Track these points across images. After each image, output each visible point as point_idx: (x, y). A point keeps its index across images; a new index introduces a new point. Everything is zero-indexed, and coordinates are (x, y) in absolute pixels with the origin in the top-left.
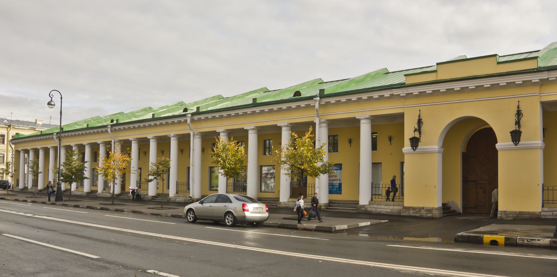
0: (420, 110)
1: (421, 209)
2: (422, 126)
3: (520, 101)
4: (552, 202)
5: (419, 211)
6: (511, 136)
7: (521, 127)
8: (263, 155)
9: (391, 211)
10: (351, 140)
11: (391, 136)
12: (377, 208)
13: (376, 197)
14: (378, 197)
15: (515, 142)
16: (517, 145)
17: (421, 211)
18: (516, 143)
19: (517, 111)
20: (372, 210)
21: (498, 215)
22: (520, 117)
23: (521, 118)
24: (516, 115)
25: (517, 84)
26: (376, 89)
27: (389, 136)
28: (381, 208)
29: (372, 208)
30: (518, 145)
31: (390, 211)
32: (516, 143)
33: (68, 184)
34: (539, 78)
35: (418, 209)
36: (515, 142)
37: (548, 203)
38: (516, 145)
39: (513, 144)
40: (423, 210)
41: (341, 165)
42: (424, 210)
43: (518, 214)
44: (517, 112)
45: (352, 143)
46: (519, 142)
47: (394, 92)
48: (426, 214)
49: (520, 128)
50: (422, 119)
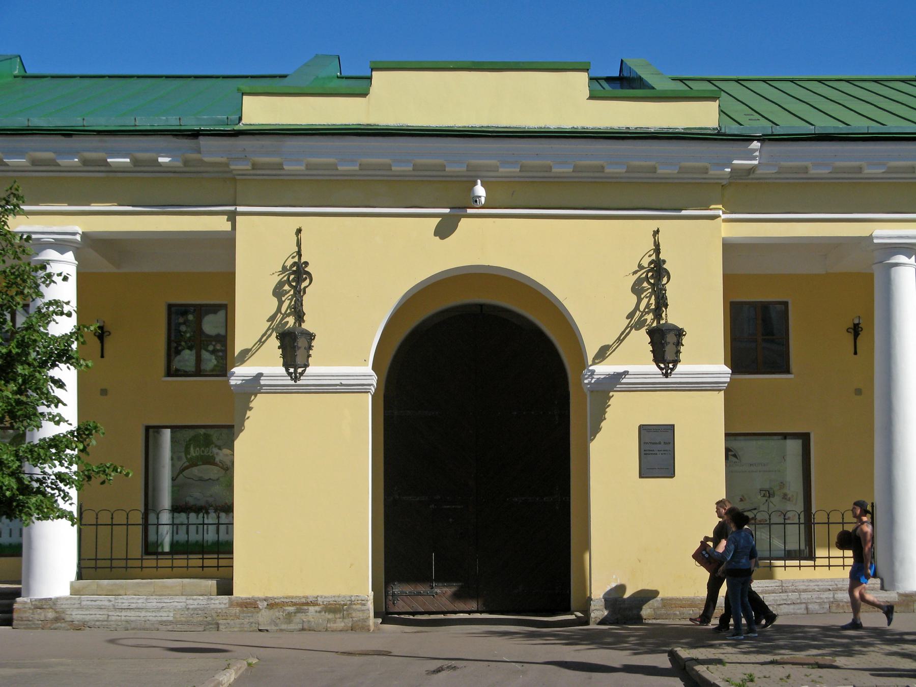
1: (307, 604)
4: (123, 563)
5: (299, 611)
6: (652, 343)
8: (165, 377)
9: (174, 617)
13: (207, 563)
14: (214, 563)
15: (662, 366)
17: (305, 612)
18: (667, 368)
20: (88, 618)
21: (593, 615)
26: (643, 136)
28: (133, 606)
29: (88, 608)
30: (672, 376)
31: (171, 619)
32: (667, 368)
35: (294, 604)
36: (662, 366)
37: (96, 568)
38: (666, 375)
39: (658, 370)
40: (312, 609)
41: (148, 428)
42: (317, 608)
43: (658, 608)
46: (675, 366)
48: (329, 621)
49: (304, 321)
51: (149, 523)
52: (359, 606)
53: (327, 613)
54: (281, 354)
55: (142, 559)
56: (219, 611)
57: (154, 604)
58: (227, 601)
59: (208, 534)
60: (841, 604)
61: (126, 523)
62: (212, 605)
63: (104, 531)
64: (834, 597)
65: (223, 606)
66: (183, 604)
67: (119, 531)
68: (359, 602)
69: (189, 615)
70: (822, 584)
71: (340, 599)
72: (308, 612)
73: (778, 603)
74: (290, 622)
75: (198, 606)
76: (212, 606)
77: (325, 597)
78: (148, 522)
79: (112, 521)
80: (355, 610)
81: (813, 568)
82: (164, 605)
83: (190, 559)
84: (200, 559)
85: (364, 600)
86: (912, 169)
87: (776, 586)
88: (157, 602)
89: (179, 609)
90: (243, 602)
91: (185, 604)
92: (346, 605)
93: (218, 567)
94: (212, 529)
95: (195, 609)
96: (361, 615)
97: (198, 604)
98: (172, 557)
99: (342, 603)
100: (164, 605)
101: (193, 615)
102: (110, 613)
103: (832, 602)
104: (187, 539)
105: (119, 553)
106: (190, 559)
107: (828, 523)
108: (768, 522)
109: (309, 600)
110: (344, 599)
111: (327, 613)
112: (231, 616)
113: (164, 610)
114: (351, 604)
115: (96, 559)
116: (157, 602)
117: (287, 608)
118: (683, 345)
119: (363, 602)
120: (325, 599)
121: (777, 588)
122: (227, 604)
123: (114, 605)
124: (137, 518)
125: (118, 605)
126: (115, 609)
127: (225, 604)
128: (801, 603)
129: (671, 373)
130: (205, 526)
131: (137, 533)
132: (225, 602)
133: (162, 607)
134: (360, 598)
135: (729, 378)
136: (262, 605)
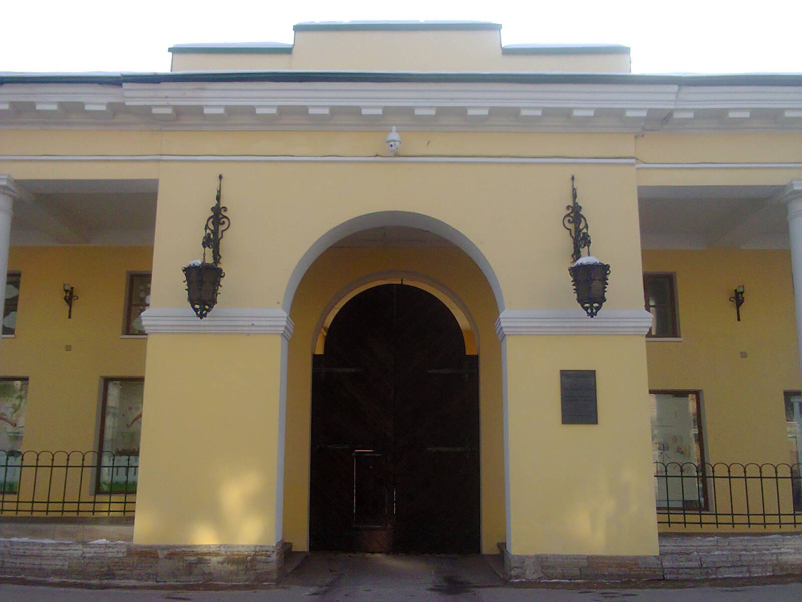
0: (221, 177)
2: (224, 233)
3: (223, 176)
7: (221, 261)
9: (69, 567)
10: (75, 293)
11: (72, 288)
12: (33, 550)
16: (205, 316)
19: (213, 209)
22: (222, 228)
23: (223, 231)
24: (208, 220)
25: (261, 115)
27: (67, 288)
28: (29, 553)
33: (574, 289)
34: (648, 106)
36: (197, 306)
44: (212, 214)
45: (75, 303)
47: (127, 94)
50: (225, 209)
51: (103, 465)
52: (264, 558)
53: (230, 565)
54: (572, 282)
55: (794, 515)
56: (116, 560)
57: (49, 552)
58: (125, 549)
59: (117, 475)
60: (785, 567)
61: (51, 465)
62: (110, 553)
63: (59, 473)
64: (777, 559)
65: (120, 555)
66: (80, 553)
67: (43, 473)
68: (264, 553)
69: (85, 564)
70: (761, 544)
71: (243, 549)
72: (210, 563)
73: (718, 565)
74: (190, 573)
75: (95, 555)
76: (110, 555)
77: (229, 547)
78: (101, 463)
79: (37, 462)
80: (260, 561)
81: (793, 525)
82: (60, 552)
83: (687, 514)
84: (698, 514)
85: (268, 551)
86: (799, 109)
87: (712, 546)
88: (52, 550)
89: (75, 558)
90: (142, 551)
91: (82, 552)
92: (249, 556)
93: (749, 524)
94: (122, 471)
95: (92, 558)
96: (36, 562)
97: (95, 553)
98: (700, 512)
99: (246, 553)
100: (60, 552)
101: (89, 565)
102: (6, 560)
103: (776, 565)
104: (125, 480)
105: (772, 508)
106: (687, 514)
107: (67, 467)
108: (664, 474)
109: (211, 550)
110: (248, 549)
111: (230, 565)
112: (129, 566)
113: (59, 558)
114: (255, 555)
115: (79, 502)
116: (52, 550)
117: (188, 558)
118: (221, 286)
119: (268, 553)
120: (229, 549)
121: (712, 547)
122: (125, 553)
123: (9, 552)
124: (90, 459)
125: (13, 552)
126: (11, 556)
127: (124, 553)
128: (741, 566)
129: (206, 313)
130: (115, 469)
131: (89, 474)
132: (123, 550)
133: (58, 555)
134: (265, 549)
135: (285, 322)
136: (161, 554)
